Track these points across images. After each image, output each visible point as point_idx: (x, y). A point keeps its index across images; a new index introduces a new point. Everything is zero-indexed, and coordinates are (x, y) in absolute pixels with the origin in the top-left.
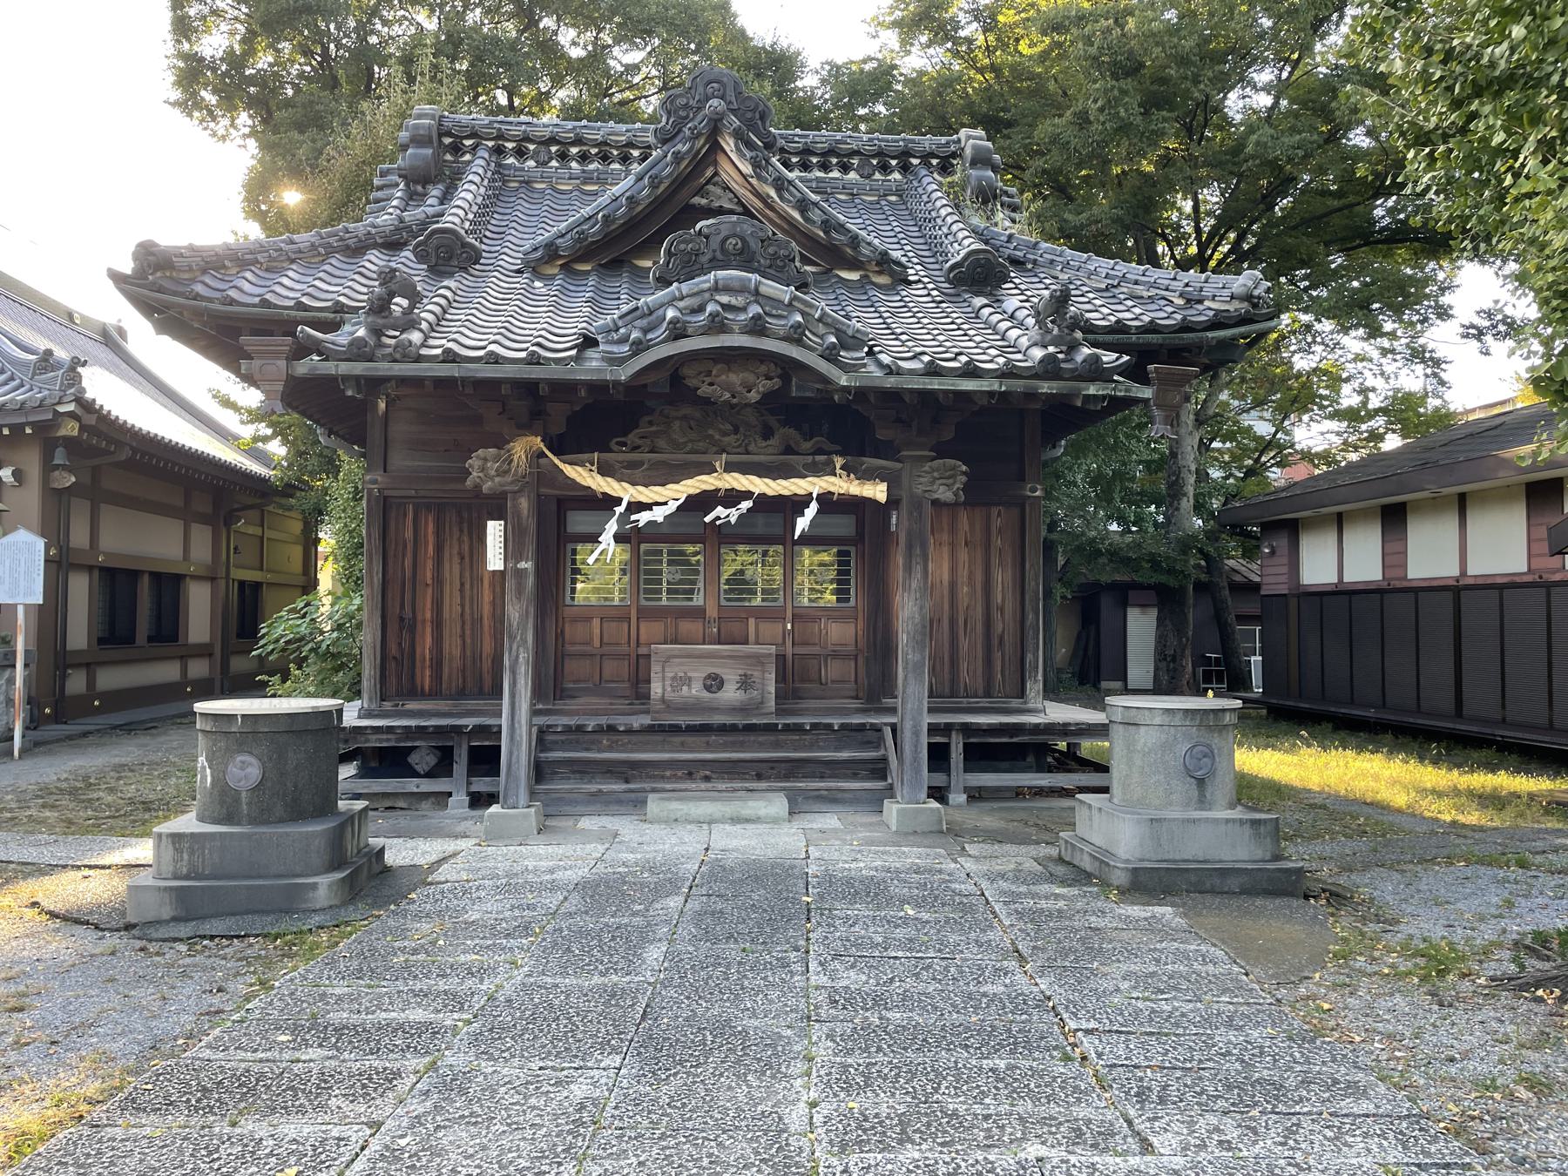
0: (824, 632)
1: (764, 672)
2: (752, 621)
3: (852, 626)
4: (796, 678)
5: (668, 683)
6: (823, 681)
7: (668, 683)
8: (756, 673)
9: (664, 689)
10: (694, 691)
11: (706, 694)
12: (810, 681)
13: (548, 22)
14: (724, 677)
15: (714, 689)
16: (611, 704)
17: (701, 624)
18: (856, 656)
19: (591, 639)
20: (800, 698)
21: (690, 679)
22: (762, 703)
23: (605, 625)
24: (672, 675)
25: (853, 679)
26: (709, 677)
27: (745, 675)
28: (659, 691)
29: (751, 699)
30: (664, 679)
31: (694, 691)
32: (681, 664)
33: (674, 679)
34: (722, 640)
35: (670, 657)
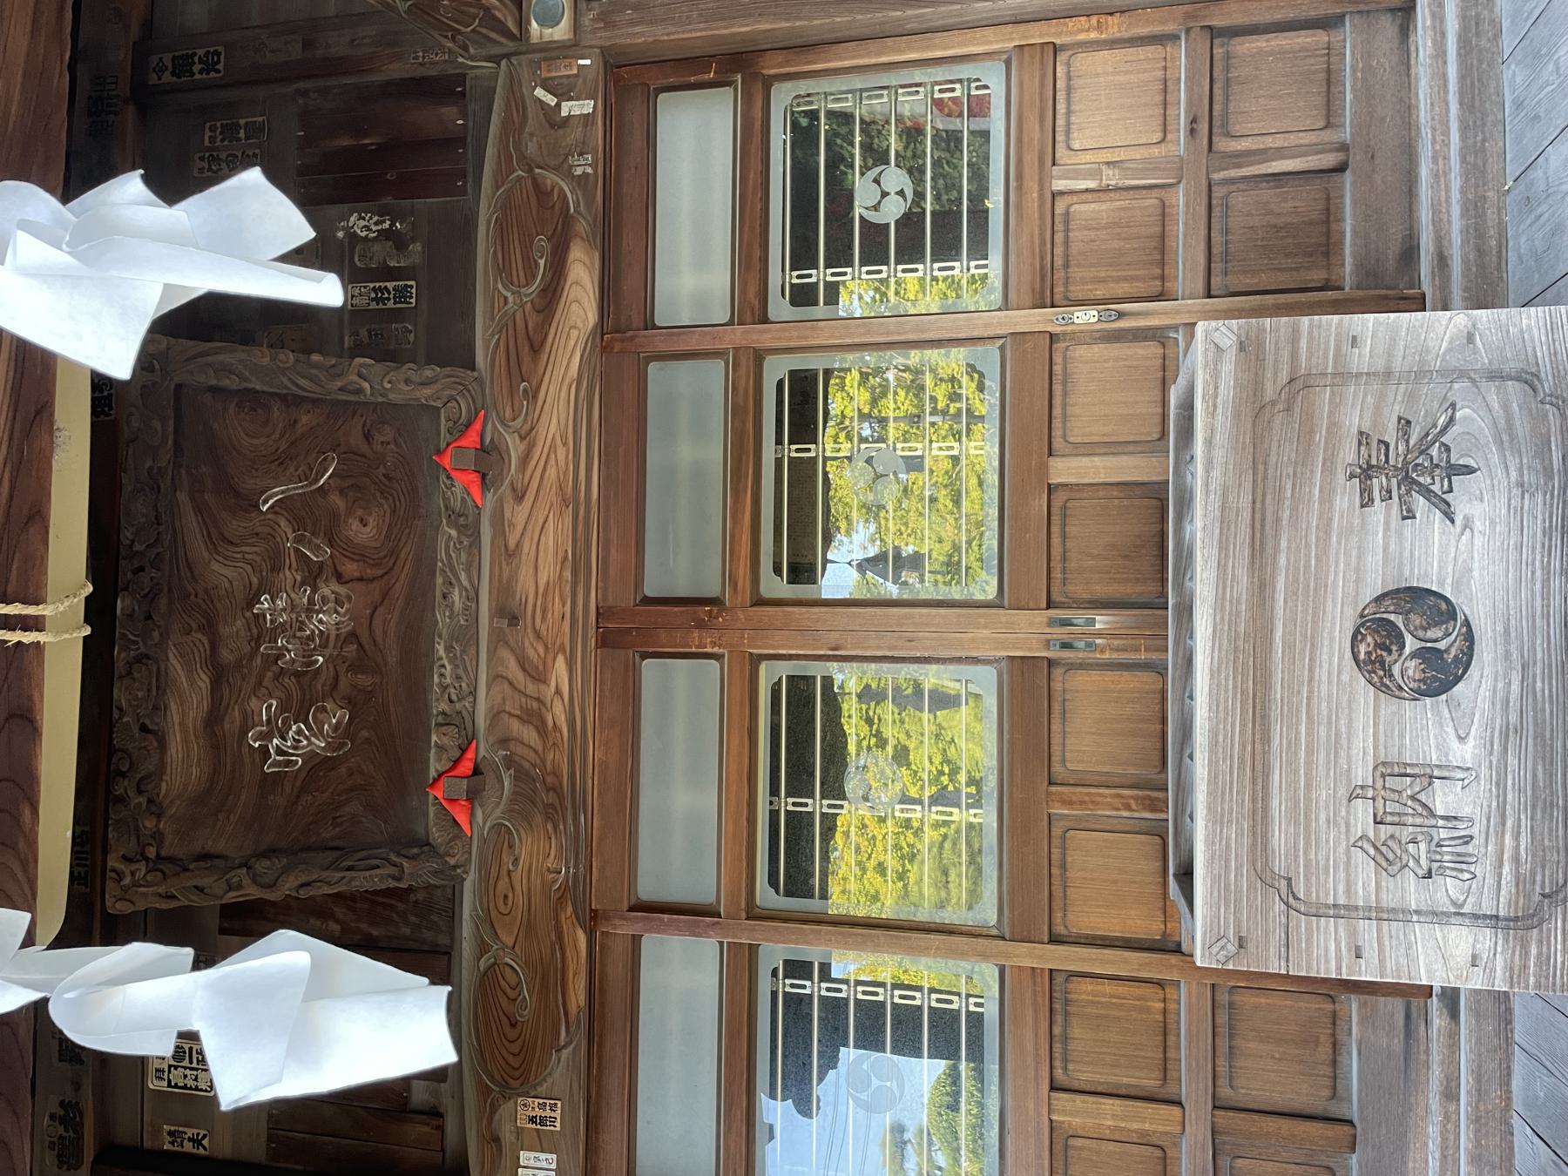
0: (1111, 178)
1: (1342, 376)
2: (1064, 470)
3: (1084, 63)
4: (1317, 276)
5: (1411, 891)
6: (1329, 160)
7: (1411, 891)
8: (1354, 420)
9: (1456, 914)
10: (1465, 753)
11: (174, 79)
12: (1329, 215)
13: (338, 715)
14: (1374, 586)
15: (1447, 642)
16: (1451, 1095)
17: (1081, 680)
18: (1213, 32)
19: (1144, 1140)
20: (1410, 254)
21: (1387, 770)
22: (1529, 379)
23: (1083, 1075)
24: (1365, 869)
25: (1321, 37)
26: (1375, 667)
27: (1366, 472)
28: (1462, 941)
29: (1505, 436)
30: (1382, 914)
31: (1465, 753)
32: (1302, 814)
33: (1387, 859)
34: (1148, 589)
35: (1264, 877)
